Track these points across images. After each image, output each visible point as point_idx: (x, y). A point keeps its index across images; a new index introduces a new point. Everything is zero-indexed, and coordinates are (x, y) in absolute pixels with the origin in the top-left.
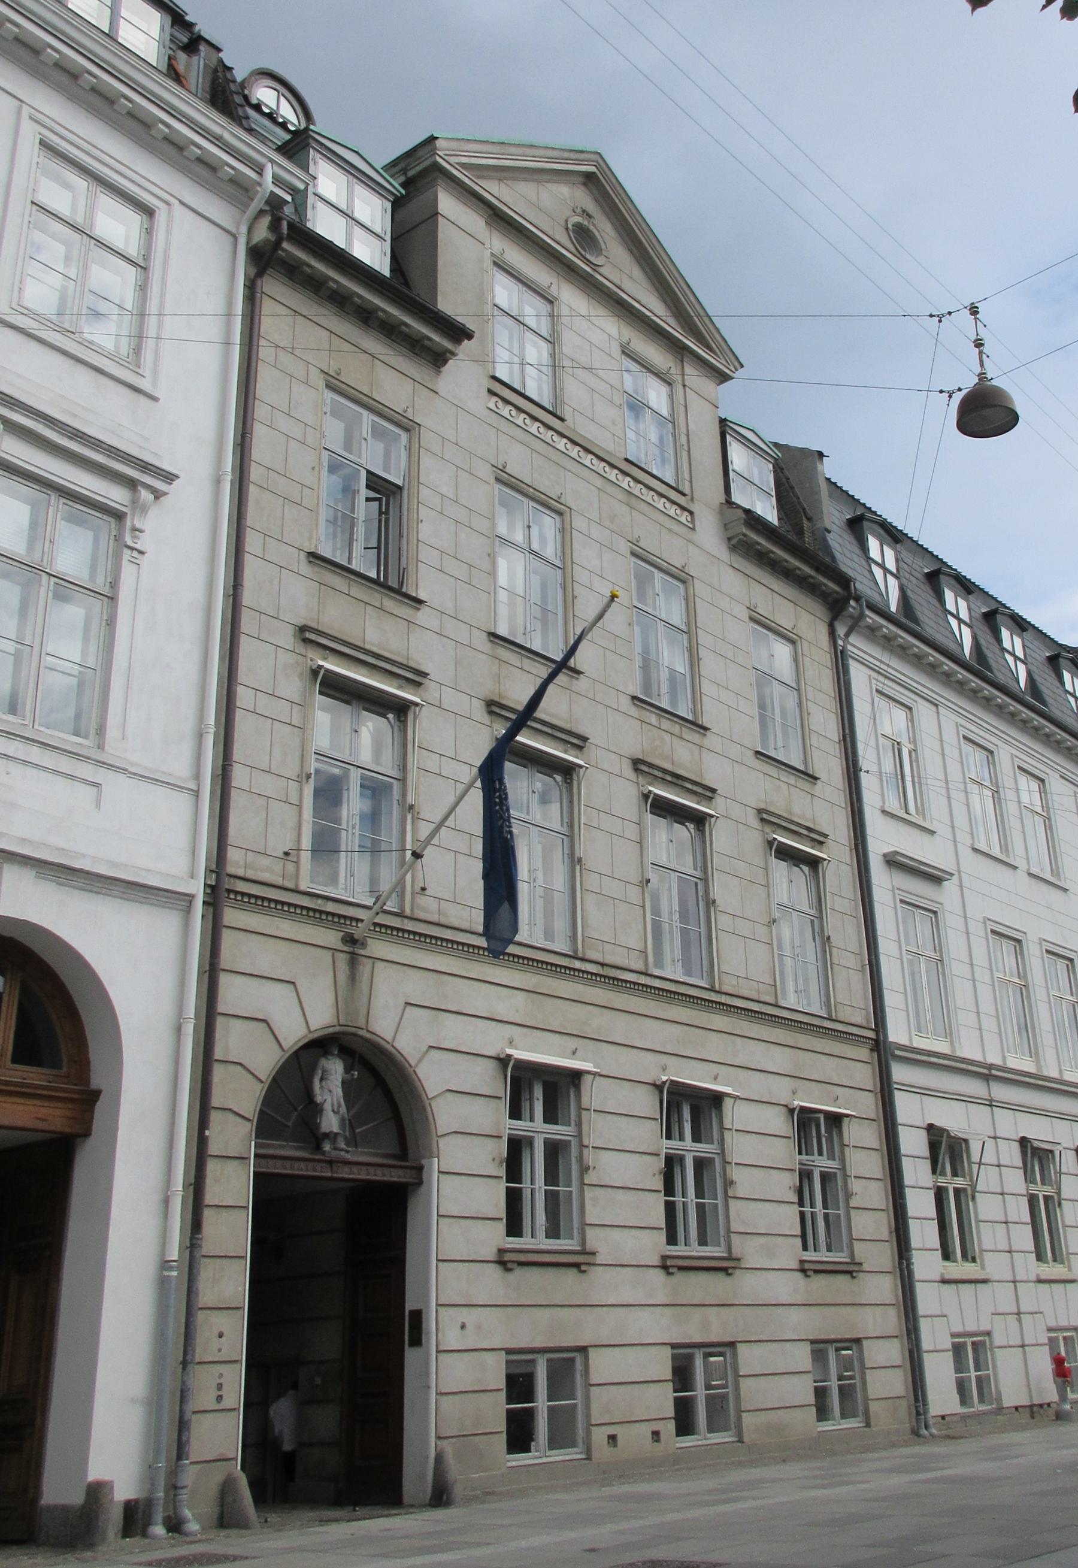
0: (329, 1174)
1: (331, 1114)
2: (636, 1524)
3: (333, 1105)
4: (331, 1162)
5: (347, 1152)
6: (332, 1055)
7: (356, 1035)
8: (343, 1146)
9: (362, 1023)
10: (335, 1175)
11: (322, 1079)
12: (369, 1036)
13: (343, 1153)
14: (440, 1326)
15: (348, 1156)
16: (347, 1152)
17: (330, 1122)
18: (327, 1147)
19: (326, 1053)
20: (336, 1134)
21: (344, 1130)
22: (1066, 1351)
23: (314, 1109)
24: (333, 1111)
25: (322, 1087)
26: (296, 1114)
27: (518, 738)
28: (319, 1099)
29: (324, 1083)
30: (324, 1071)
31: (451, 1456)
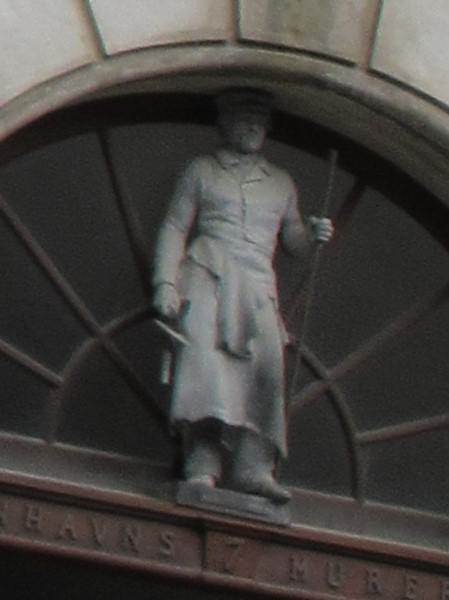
0: (191, 570)
1: (216, 359)
2: (356, 536)
3: (221, 325)
4: (199, 528)
5: (278, 501)
6: (242, 151)
7: (320, 84)
8: (265, 476)
9: (343, 39)
10: (213, 575)
11: (194, 233)
12: (376, 90)
13: (256, 504)
14: (212, 38)
15: (282, 517)
16: (278, 501)
17: (210, 386)
18: (203, 474)
19: (224, 145)
20: (239, 432)
21: (263, 417)
22: (56, 448)
23: (150, 339)
24: (223, 347)
25: (187, 261)
26: (88, 343)
27: (444, 417)
28: (168, 300)
29: (196, 252)
30: (202, 206)
31: (365, 471)
